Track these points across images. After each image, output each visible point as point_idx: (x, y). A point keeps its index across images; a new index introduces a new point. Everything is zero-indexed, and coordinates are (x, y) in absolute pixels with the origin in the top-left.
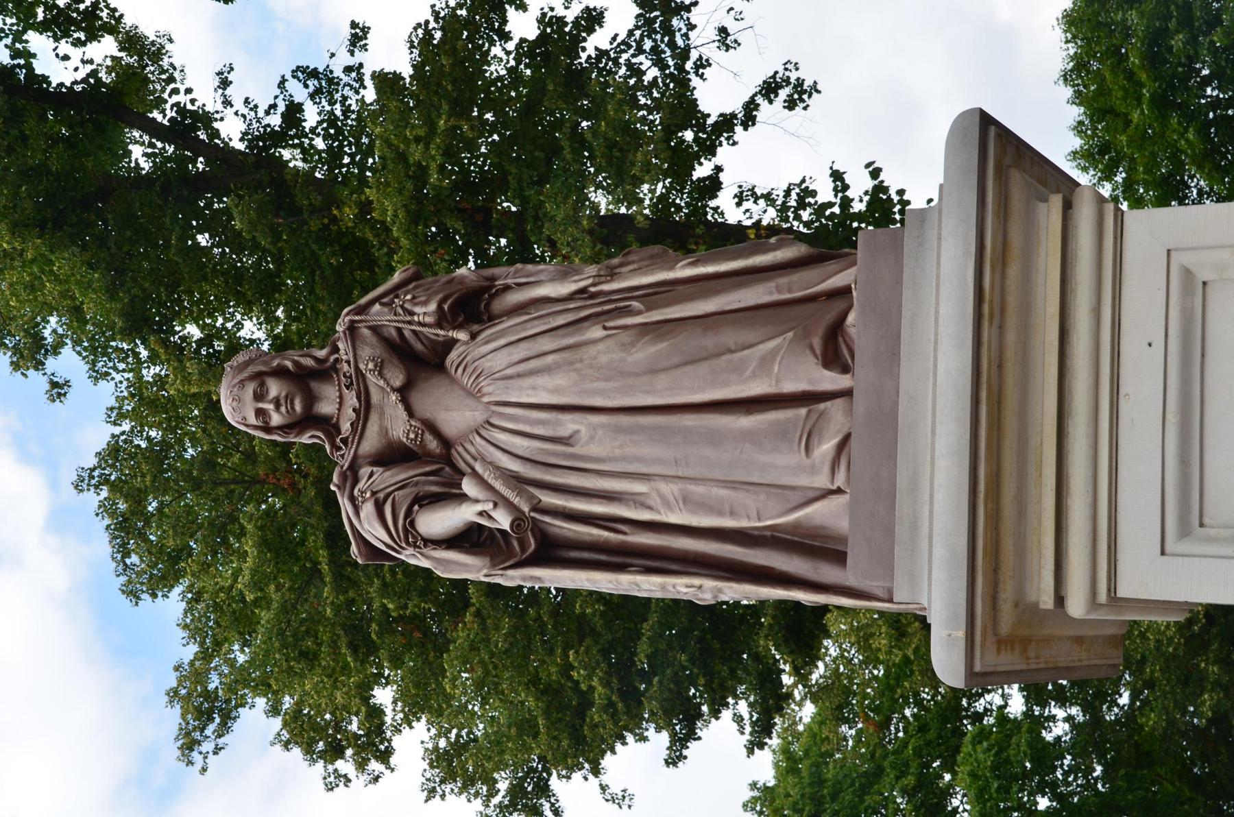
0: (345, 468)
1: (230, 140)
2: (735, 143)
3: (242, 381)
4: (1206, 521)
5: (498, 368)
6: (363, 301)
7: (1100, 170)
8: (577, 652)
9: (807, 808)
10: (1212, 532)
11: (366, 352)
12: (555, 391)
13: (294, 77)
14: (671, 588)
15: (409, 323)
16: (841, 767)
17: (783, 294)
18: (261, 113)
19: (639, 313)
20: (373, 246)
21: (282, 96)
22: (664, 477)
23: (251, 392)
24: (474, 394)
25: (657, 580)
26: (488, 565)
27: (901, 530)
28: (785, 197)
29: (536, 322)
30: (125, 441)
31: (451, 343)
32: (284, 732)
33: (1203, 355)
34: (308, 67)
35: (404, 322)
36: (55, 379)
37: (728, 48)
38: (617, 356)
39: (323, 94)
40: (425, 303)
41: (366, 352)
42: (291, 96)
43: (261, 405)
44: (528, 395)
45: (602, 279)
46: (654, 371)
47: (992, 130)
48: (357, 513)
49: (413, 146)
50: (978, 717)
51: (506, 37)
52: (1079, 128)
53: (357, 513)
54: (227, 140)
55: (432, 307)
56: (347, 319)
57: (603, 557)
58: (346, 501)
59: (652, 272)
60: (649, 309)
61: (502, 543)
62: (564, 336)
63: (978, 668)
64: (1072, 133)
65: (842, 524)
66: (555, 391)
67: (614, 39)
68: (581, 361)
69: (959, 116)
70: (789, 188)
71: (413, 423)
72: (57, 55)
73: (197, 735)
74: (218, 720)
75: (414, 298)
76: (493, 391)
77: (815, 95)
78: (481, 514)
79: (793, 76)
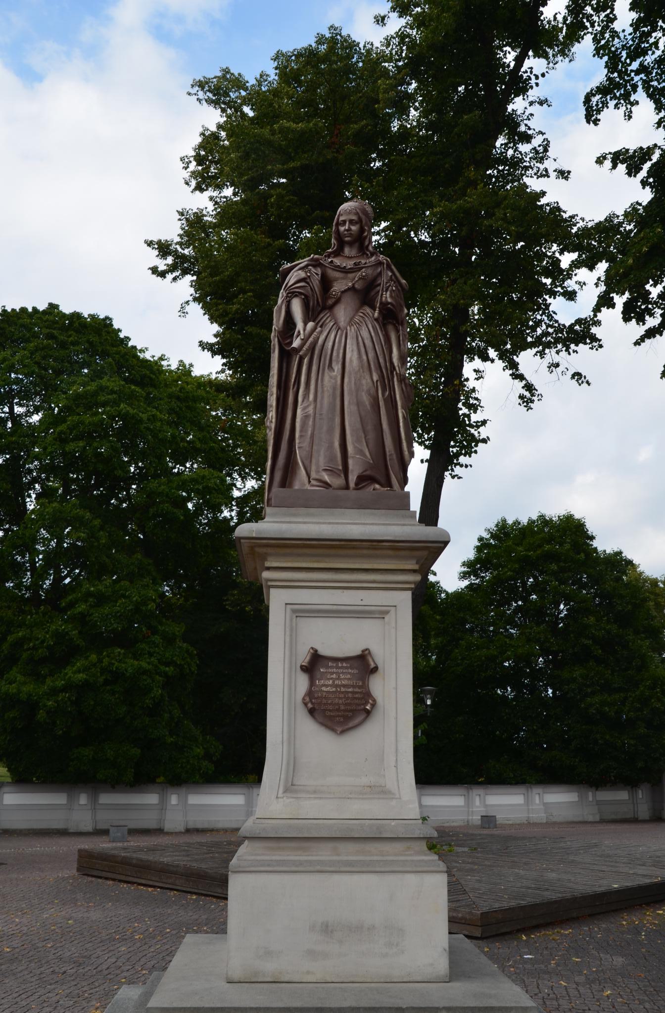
1: (513, 103)
2: (504, 370)
4: (298, 618)
6: (393, 267)
7: (496, 533)
8: (251, 296)
9: (182, 395)
10: (294, 620)
11: (370, 271)
12: (351, 360)
13: (544, 139)
14: (271, 409)
15: (383, 289)
16: (202, 410)
18: (525, 122)
19: (383, 395)
20: (454, 186)
21: (535, 133)
24: (351, 322)
25: (274, 404)
27: (293, 510)
28: (475, 398)
29: (381, 349)
30: (356, 50)
31: (373, 308)
32: (209, 132)
33: (358, 617)
34: (549, 147)
36: (386, 18)
37: (549, 367)
38: (365, 388)
39: (536, 154)
40: (391, 296)
41: (370, 271)
42: (535, 138)
43: (347, 223)
46: (359, 404)
47: (443, 545)
49: (502, 212)
50: (230, 475)
51: (561, 253)
52: (517, 523)
54: (513, 101)
55: (389, 300)
57: (283, 378)
58: (306, 263)
59: (401, 399)
60: (385, 400)
61: (289, 335)
62: (374, 362)
63: (242, 541)
64: (515, 519)
65: (297, 486)
66: (351, 360)
67: (555, 313)
68: (363, 372)
69: (446, 532)
70: (479, 399)
72: (556, 14)
73: (207, 88)
74: (214, 98)
75: (394, 291)
76: (352, 331)
77: (526, 409)
78: (299, 332)
79: (535, 398)
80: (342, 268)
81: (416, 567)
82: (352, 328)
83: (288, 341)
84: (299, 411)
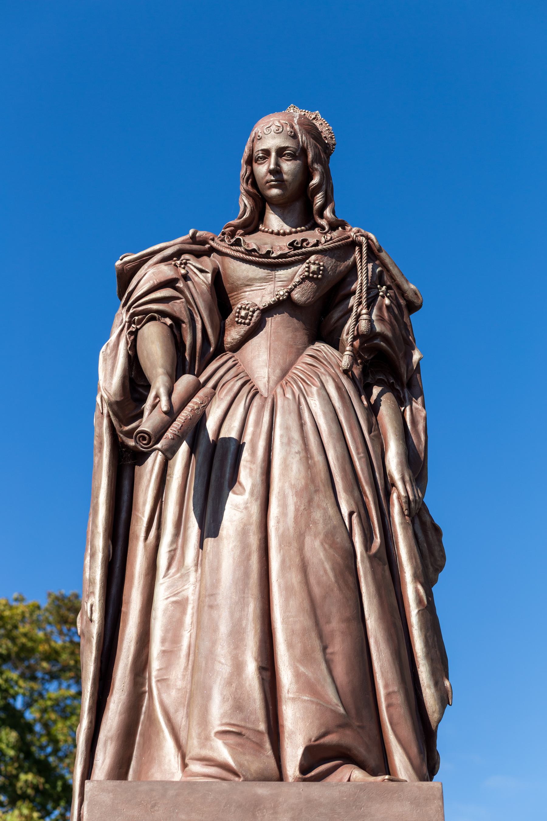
0: (211, 242)
23: (287, 145)
26: (113, 399)
29: (359, 440)
48: (164, 260)
53: (164, 260)
56: (363, 239)
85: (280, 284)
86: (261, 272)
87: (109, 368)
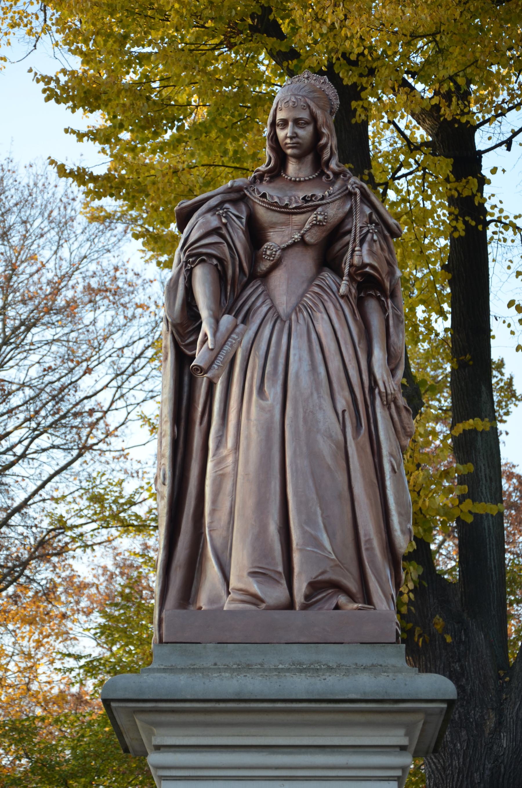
0: (246, 191)
3: (309, 107)
5: (316, 325)
15: (355, 240)
17: (365, 545)
22: (236, 462)
23: (300, 116)
35: (355, 235)
43: (290, 124)
44: (295, 355)
45: (385, 399)
48: (210, 210)
55: (367, 260)
56: (358, 191)
63: (113, 705)
71: (278, 253)
78: (206, 335)
80: (281, 207)
81: (404, 741)
82: (300, 316)
83: (192, 339)
84: (210, 465)
85: (296, 227)
86: (282, 218)
87: (172, 298)
